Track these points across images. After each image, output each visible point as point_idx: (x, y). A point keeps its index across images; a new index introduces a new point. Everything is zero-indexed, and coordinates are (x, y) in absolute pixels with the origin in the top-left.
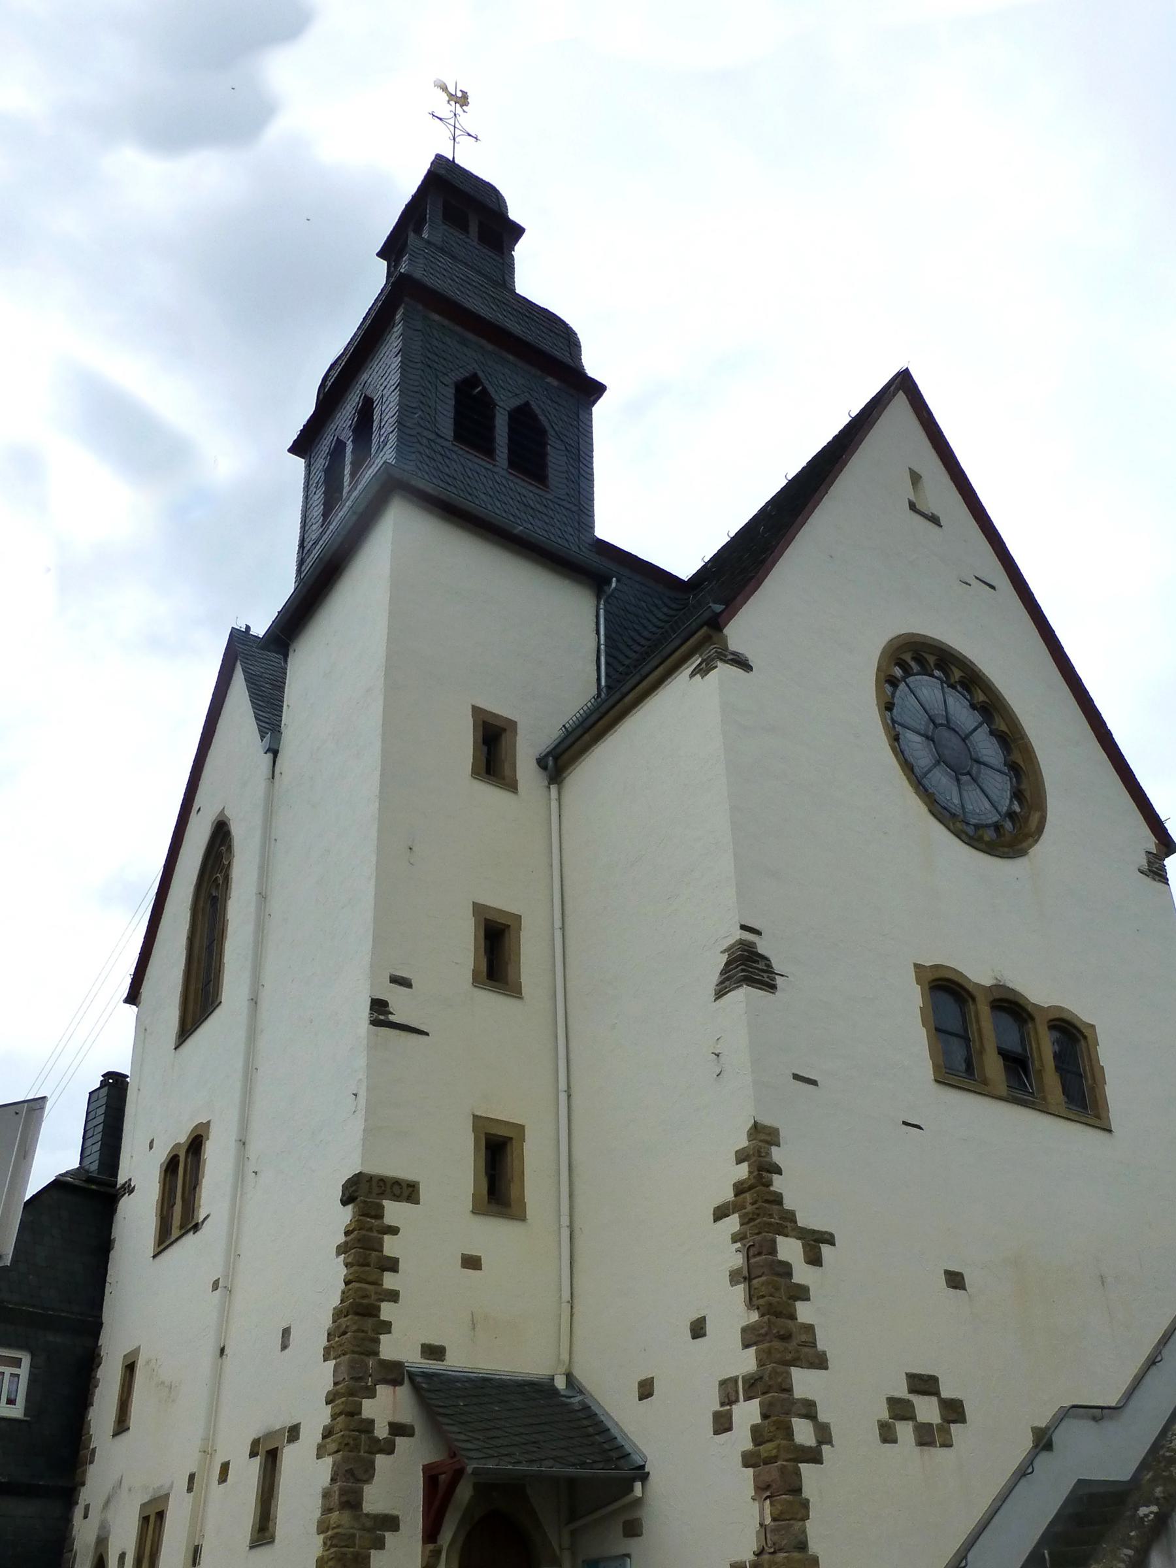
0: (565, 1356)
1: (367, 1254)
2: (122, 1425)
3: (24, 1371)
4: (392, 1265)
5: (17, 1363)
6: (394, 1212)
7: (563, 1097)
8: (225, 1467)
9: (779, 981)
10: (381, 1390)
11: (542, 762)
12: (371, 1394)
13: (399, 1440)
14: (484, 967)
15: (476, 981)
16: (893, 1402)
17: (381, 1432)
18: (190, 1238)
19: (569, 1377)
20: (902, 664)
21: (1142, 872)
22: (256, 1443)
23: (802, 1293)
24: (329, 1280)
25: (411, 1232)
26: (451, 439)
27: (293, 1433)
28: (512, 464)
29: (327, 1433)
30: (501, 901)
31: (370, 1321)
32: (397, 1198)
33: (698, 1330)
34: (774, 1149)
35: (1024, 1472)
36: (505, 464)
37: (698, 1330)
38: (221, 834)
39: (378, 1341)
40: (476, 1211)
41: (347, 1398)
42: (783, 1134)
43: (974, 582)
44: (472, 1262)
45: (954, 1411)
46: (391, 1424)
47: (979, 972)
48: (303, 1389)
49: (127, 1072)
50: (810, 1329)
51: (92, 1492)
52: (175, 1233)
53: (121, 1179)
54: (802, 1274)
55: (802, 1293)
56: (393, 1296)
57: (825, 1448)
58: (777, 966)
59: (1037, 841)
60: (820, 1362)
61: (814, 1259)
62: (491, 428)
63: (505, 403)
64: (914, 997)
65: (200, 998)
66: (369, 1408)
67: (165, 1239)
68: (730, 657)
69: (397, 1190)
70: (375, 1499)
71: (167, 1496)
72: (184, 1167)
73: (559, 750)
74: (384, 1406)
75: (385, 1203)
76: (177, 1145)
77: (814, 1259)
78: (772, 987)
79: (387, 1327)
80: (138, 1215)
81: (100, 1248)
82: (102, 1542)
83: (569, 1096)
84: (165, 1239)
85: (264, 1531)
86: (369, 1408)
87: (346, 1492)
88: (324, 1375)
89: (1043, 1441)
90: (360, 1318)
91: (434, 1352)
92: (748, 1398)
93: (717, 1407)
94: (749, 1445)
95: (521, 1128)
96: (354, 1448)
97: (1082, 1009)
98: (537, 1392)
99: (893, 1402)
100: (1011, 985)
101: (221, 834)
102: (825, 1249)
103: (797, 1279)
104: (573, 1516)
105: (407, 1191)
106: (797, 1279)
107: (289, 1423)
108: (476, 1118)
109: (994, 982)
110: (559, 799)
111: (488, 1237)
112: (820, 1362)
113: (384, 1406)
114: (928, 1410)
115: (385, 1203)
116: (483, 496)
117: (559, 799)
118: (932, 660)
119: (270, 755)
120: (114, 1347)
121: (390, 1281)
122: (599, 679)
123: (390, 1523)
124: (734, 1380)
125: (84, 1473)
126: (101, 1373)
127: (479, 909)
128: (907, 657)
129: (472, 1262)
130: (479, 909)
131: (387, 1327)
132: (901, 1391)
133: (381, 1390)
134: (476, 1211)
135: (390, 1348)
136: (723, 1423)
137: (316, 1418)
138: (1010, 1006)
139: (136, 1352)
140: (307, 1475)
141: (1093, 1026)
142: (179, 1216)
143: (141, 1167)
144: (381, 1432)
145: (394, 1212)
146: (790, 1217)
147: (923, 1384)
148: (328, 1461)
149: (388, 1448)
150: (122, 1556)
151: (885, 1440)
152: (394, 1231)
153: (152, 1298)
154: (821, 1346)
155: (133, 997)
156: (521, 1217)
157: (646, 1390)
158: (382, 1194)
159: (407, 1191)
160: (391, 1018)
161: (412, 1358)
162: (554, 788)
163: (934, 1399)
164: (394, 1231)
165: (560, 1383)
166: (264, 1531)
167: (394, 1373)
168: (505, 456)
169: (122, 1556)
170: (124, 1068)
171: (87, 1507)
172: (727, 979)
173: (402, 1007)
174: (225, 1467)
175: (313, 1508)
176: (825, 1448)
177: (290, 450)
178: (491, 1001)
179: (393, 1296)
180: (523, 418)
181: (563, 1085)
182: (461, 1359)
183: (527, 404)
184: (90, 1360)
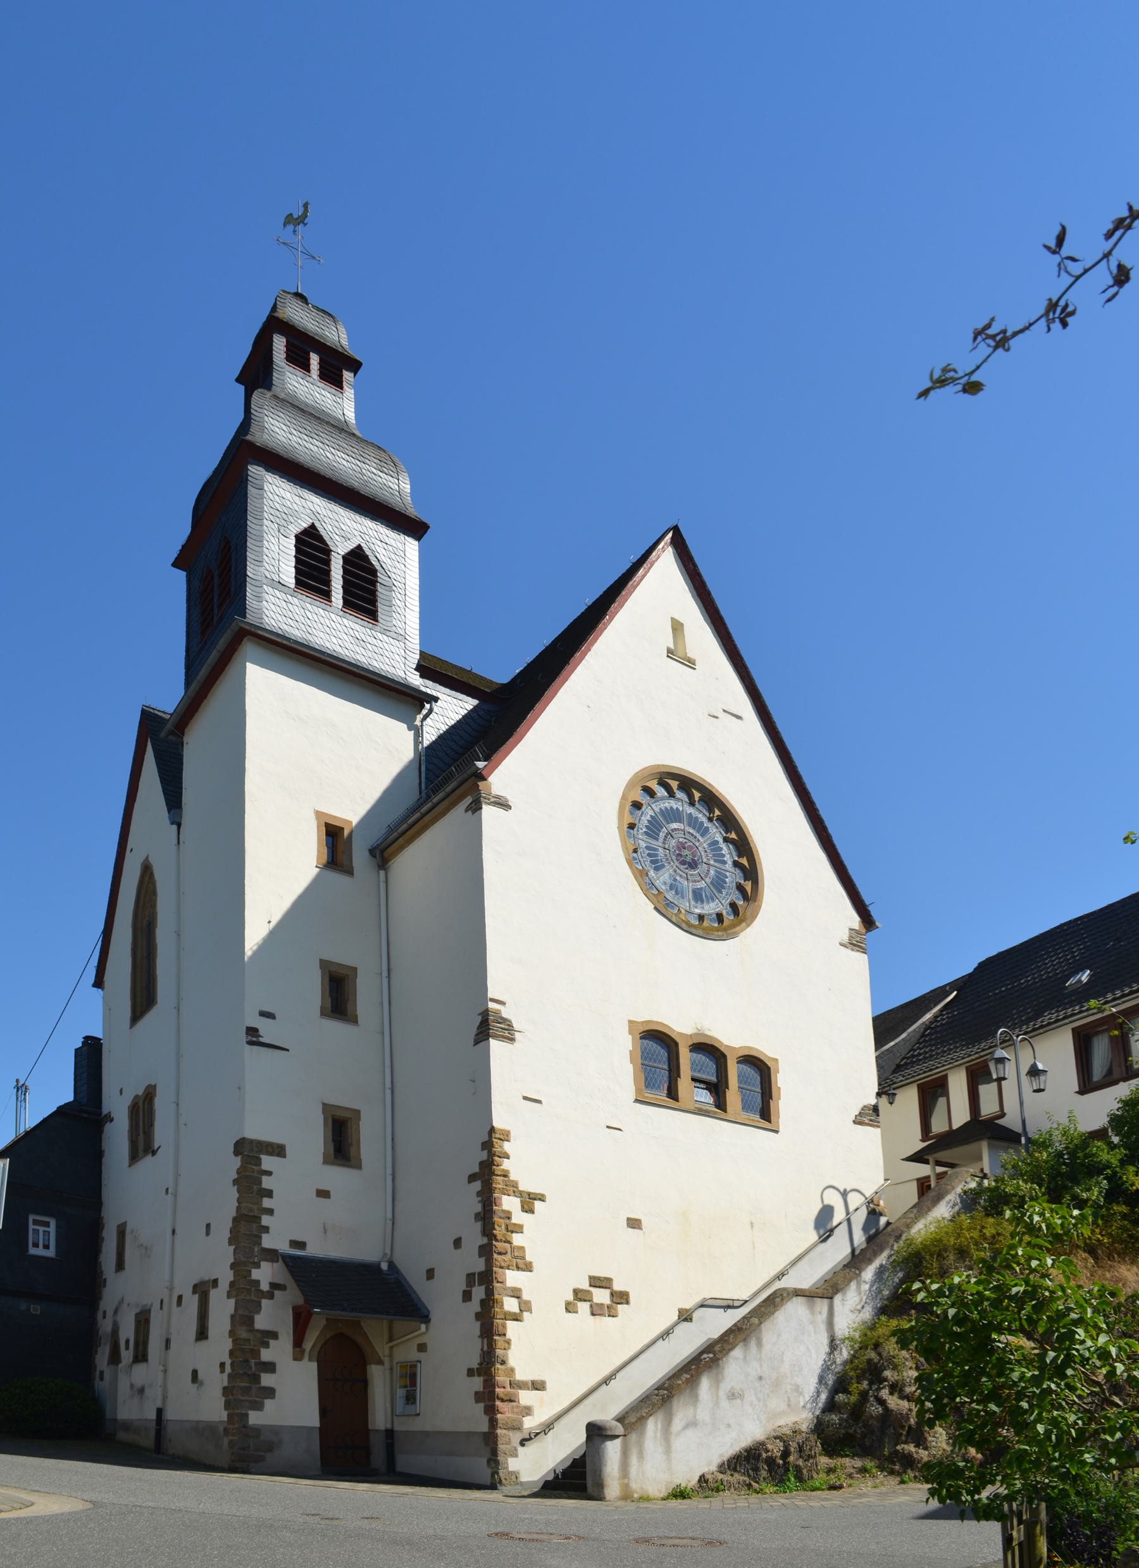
0: (388, 1252)
1: (251, 1185)
2: (120, 1266)
3: (52, 1229)
4: (269, 1194)
5: (47, 1224)
6: (268, 1162)
7: (388, 1092)
8: (180, 1298)
9: (517, 1035)
10: (263, 1264)
11: (372, 852)
12: (258, 1266)
13: (276, 1292)
14: (329, 1005)
15: (323, 1014)
16: (576, 1292)
17: (265, 1287)
18: (149, 1157)
19: (391, 1265)
20: (650, 792)
21: (842, 945)
22: (195, 1286)
23: (519, 1229)
24: (227, 1203)
25: (280, 1176)
26: (293, 586)
27: (215, 1283)
28: (347, 604)
29: (232, 1284)
30: (342, 957)
31: (254, 1226)
32: (271, 1154)
33: (457, 1243)
34: (506, 1144)
35: (666, 1334)
36: (341, 602)
37: (457, 1243)
38: (147, 870)
39: (260, 1238)
40: (326, 1162)
41: (241, 1268)
42: (512, 1134)
43: (721, 715)
44: (323, 1194)
45: (621, 1298)
46: (271, 1284)
47: (682, 1024)
48: (217, 1259)
49: (100, 1036)
50: (522, 1249)
51: (108, 1302)
52: (141, 1153)
53: (105, 1111)
54: (519, 1217)
55: (519, 1229)
56: (270, 1212)
57: (526, 1314)
58: (516, 1026)
59: (748, 925)
60: (528, 1267)
61: (528, 1209)
62: (328, 573)
63: (340, 548)
64: (625, 1043)
65: (143, 998)
66: (256, 1274)
67: (134, 1157)
68: (493, 800)
69: (270, 1150)
70: (262, 1322)
71: (150, 1310)
72: (143, 1110)
73: (384, 845)
74: (264, 1274)
75: (262, 1156)
76: (137, 1096)
77: (528, 1209)
78: (512, 1040)
79: (266, 1229)
80: (117, 1136)
81: (95, 1155)
82: (115, 1331)
83: (393, 1092)
84: (134, 1157)
85: (202, 1334)
86: (256, 1274)
87: (243, 1319)
88: (228, 1254)
89: (685, 1316)
90: (247, 1225)
91: (299, 1245)
92: (480, 1285)
93: (465, 1288)
94: (479, 1309)
95: (357, 1113)
96: (247, 1295)
97: (766, 1049)
98: (371, 1269)
99: (576, 1292)
100: (709, 1033)
101: (147, 870)
102: (537, 1204)
103: (514, 1220)
104: (391, 1339)
105: (278, 1150)
106: (514, 1220)
107: (213, 1278)
108: (324, 1105)
109: (695, 1031)
110: (386, 882)
111: (337, 1177)
112: (528, 1267)
113: (264, 1274)
114: (601, 1296)
115: (262, 1156)
116: (321, 634)
117: (386, 882)
118: (674, 784)
119: (175, 827)
120: (112, 1217)
121: (266, 1203)
122: (420, 784)
123: (274, 1335)
124: (474, 1274)
125: (100, 1292)
126: (105, 1234)
127: (324, 964)
128: (654, 785)
129: (323, 1194)
130: (324, 964)
131: (266, 1229)
132: (585, 1285)
133: (263, 1264)
134: (326, 1162)
135: (267, 1242)
136: (467, 1296)
137: (226, 1276)
138: (707, 1049)
139: (125, 1224)
140: (222, 1308)
141: (776, 1060)
142: (142, 1144)
143: (117, 1103)
144: (265, 1287)
145: (268, 1162)
146: (515, 1185)
147: (598, 1282)
148: (232, 1301)
149: (270, 1295)
150: (127, 1341)
151: (568, 1311)
152: (269, 1173)
153: (133, 1193)
154: (528, 1259)
155: (99, 983)
156: (358, 1166)
157: (430, 1274)
158: (261, 1152)
159: (278, 1150)
160: (261, 1040)
161: (284, 1248)
162: (382, 873)
163: (608, 1291)
164: (269, 1173)
165: (384, 1266)
166: (202, 1334)
167: (272, 1255)
168: (340, 596)
169: (127, 1341)
170: (99, 1034)
171: (105, 1312)
172: (481, 1033)
173: (268, 1031)
174: (180, 1298)
175: (227, 1325)
176: (526, 1314)
177: (174, 565)
178: (335, 1028)
179: (270, 1212)
180: (358, 561)
181: (388, 1084)
182: (314, 1250)
183: (359, 547)
184: (96, 1226)
